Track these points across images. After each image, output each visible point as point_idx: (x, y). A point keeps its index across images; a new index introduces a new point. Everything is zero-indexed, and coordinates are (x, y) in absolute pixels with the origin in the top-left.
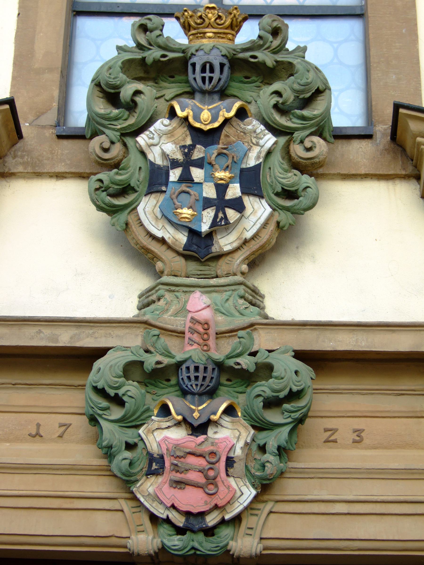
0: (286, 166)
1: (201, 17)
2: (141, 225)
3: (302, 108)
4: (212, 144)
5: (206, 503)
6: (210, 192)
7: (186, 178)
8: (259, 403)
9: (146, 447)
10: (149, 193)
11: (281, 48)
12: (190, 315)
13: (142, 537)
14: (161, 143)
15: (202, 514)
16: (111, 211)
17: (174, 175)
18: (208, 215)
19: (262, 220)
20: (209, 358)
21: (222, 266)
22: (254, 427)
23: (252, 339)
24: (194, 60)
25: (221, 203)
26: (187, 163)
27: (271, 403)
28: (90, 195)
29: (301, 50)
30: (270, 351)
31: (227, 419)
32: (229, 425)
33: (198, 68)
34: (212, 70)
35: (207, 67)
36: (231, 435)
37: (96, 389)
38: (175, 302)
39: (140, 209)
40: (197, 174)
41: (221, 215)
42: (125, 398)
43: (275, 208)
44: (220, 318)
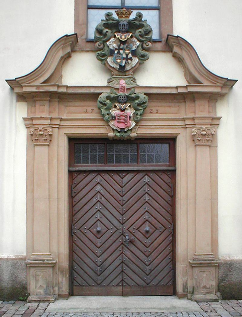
0: (142, 50)
1: (122, 12)
2: (108, 63)
3: (146, 35)
4: (125, 44)
5: (125, 126)
6: (124, 56)
7: (119, 53)
8: (136, 105)
9: (111, 114)
10: (110, 56)
11: (141, 20)
12: (121, 85)
13: (111, 133)
14: (112, 44)
15: (124, 128)
16: (101, 60)
17: (116, 52)
18: (124, 61)
19: (136, 62)
20: (125, 95)
21: (127, 73)
22: (135, 110)
23: (135, 91)
24: (120, 23)
25: (127, 59)
26: (119, 49)
27: (139, 105)
28: (96, 57)
29: (146, 21)
30: (139, 93)
31: (129, 108)
32: (130, 109)
33: (121, 25)
34: (125, 26)
35: (123, 25)
36: (130, 112)
37: (100, 102)
38: (116, 82)
39: (108, 60)
40: (121, 52)
41: (127, 61)
42: (107, 104)
43: (139, 59)
44: (127, 85)
